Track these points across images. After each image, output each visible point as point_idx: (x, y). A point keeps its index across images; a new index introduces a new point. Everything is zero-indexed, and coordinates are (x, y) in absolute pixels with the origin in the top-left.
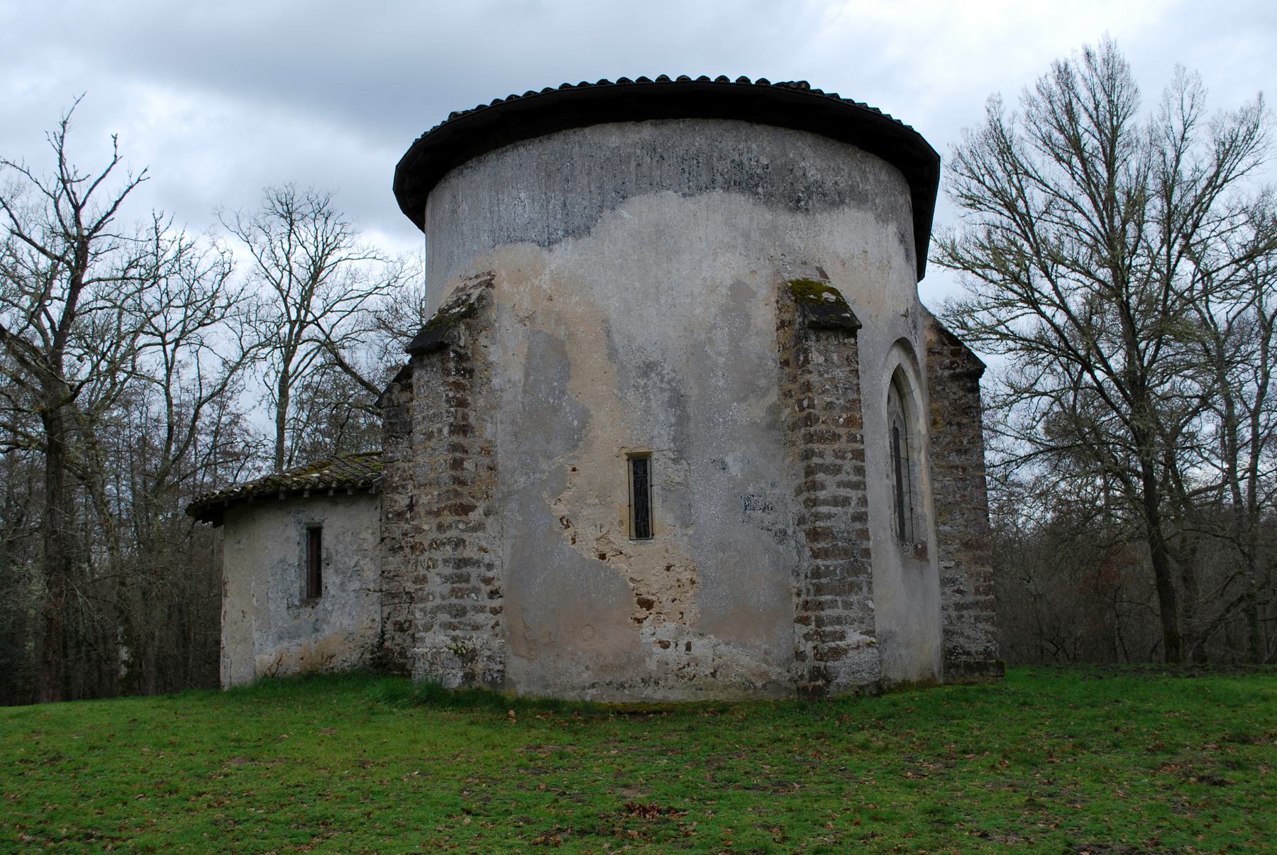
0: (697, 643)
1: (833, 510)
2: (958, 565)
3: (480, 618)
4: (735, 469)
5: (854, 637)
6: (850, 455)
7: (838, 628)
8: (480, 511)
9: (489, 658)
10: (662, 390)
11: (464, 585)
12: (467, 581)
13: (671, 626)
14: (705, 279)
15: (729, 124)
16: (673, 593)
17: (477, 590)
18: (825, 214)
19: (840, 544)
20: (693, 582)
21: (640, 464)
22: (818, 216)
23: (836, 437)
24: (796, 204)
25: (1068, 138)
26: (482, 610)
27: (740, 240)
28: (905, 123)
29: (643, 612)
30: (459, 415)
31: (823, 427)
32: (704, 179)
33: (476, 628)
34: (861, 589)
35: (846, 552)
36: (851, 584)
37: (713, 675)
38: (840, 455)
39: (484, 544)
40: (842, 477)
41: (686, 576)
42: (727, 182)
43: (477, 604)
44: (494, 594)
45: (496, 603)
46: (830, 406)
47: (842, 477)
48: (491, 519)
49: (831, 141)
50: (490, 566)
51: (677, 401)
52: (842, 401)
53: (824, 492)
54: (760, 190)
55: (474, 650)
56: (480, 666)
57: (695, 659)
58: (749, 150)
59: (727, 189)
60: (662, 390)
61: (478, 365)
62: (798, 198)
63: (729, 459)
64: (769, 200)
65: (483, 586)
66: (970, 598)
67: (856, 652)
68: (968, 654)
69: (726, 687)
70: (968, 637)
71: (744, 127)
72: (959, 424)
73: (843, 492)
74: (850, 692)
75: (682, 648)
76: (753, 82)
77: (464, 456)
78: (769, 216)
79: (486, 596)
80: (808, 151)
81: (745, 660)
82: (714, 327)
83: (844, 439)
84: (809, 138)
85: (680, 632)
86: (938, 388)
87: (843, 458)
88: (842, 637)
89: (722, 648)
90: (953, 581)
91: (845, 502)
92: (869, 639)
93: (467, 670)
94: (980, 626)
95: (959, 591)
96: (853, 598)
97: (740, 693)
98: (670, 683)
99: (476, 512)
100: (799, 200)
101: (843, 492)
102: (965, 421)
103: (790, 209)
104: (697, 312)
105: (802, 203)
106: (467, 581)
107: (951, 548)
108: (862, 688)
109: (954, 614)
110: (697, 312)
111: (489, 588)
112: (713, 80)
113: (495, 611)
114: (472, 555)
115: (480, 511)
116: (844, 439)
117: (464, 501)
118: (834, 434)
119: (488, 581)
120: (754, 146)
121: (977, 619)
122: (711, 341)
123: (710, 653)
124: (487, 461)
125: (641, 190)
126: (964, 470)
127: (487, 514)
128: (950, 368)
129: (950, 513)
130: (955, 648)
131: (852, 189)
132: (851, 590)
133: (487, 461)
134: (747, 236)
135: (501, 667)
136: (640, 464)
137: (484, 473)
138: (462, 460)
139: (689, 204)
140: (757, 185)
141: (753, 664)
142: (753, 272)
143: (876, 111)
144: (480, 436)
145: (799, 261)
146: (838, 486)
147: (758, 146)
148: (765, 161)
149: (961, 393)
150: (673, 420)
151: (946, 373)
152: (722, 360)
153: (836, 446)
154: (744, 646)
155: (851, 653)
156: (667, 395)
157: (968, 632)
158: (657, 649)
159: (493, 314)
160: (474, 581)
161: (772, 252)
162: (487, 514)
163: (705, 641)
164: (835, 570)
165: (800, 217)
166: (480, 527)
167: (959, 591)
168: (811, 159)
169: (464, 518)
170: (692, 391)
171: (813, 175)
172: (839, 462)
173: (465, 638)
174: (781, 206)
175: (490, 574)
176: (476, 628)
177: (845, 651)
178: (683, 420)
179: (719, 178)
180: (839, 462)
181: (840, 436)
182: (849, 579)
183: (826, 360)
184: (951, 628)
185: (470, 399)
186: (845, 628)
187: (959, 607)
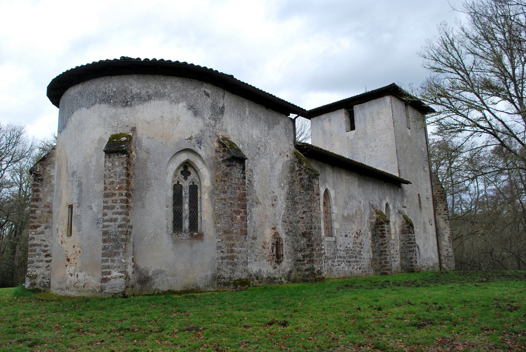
0: (80, 274)
1: (110, 223)
2: (222, 240)
3: (40, 264)
4: (95, 209)
5: (115, 273)
6: (119, 201)
7: (108, 270)
8: (43, 227)
9: (43, 278)
10: (77, 181)
11: (33, 253)
12: (35, 251)
13: (73, 268)
14: (91, 139)
15: (103, 78)
16: (74, 256)
17: (39, 255)
18: (140, 105)
19: (112, 237)
20: (80, 252)
21: (71, 207)
22: (137, 107)
23: (114, 195)
24: (126, 104)
25: (484, 37)
26: (42, 261)
27: (103, 122)
28: (189, 63)
29: (67, 263)
30: (35, 195)
31: (109, 191)
32: (93, 101)
33: (38, 267)
34: (119, 255)
35: (114, 240)
36: (115, 253)
37: (84, 286)
38: (115, 202)
39: (44, 238)
40: (115, 210)
41: (78, 249)
42: (100, 100)
43: (38, 259)
44: (47, 256)
45: (48, 259)
46: (112, 183)
47: (115, 210)
48: (47, 230)
49: (158, 77)
50: (46, 246)
51: (80, 185)
52: (118, 180)
53: (106, 217)
54: (112, 101)
55: (36, 275)
56: (38, 281)
57: (79, 280)
58: (109, 87)
59: (100, 103)
60: (77, 181)
61: (45, 177)
62: (127, 101)
63: (93, 206)
64: (115, 105)
65: (42, 253)
66: (226, 255)
67: (114, 280)
68: (224, 278)
69: (87, 291)
70: (224, 271)
71: (108, 78)
72: (224, 181)
73: (115, 216)
74: (110, 296)
75: (76, 276)
76: (142, 60)
77: (36, 209)
78: (114, 110)
79: (43, 256)
80: (134, 82)
81: (94, 281)
82: (92, 156)
83: (117, 195)
84: (135, 77)
85: (75, 270)
86: (218, 166)
87: (116, 203)
88: (110, 273)
89: (87, 276)
90: (220, 247)
91: (116, 220)
92: (121, 274)
93: (32, 282)
94: (229, 266)
95: (222, 252)
96: (116, 258)
97: (91, 294)
98: (72, 289)
99: (41, 228)
100: (128, 102)
101: (115, 216)
102: (226, 179)
103: (123, 106)
104: (88, 151)
105: (129, 103)
106: (35, 251)
107: (220, 233)
108: (115, 294)
109: (220, 261)
110: (88, 151)
111: (45, 254)
112: (142, 60)
113: (47, 262)
114: (37, 242)
115: (43, 227)
116: (117, 195)
117: (35, 224)
118: (113, 193)
119: (45, 251)
120: (111, 85)
121: (227, 263)
122: (91, 161)
123: (83, 278)
124: (48, 210)
125: (77, 109)
126: (225, 200)
127: (45, 228)
128: (223, 157)
129: (220, 218)
130: (220, 275)
131: (156, 93)
132: (115, 255)
133: (48, 210)
134: (105, 120)
135: (48, 281)
136: (71, 207)
137: (46, 214)
138: (35, 211)
139: (89, 111)
140: (111, 100)
141: (96, 283)
142: (106, 133)
143: (68, 71)
144: (45, 201)
145: (124, 126)
146: (113, 214)
147: (111, 85)
148: (114, 90)
149: (225, 167)
150: (78, 192)
151: (221, 159)
152: (93, 168)
153: (114, 198)
154: (93, 276)
155: (112, 280)
156: (77, 183)
157: (224, 269)
158: (69, 276)
159: (53, 159)
160: (38, 251)
161: (113, 124)
162: (45, 228)
163: (82, 274)
164: (108, 247)
165: (127, 109)
166: (42, 232)
167: (222, 252)
168: (134, 85)
169: (35, 230)
170: (84, 181)
171: (135, 90)
172: (114, 204)
173: (32, 271)
174: (119, 106)
175: (46, 249)
176: (38, 267)
177: (110, 279)
178: (81, 191)
179: (98, 100)
180: (114, 204)
181: (115, 194)
182: (115, 251)
183: (113, 165)
184: (219, 267)
185: (40, 189)
186: (111, 270)
187: (222, 258)
